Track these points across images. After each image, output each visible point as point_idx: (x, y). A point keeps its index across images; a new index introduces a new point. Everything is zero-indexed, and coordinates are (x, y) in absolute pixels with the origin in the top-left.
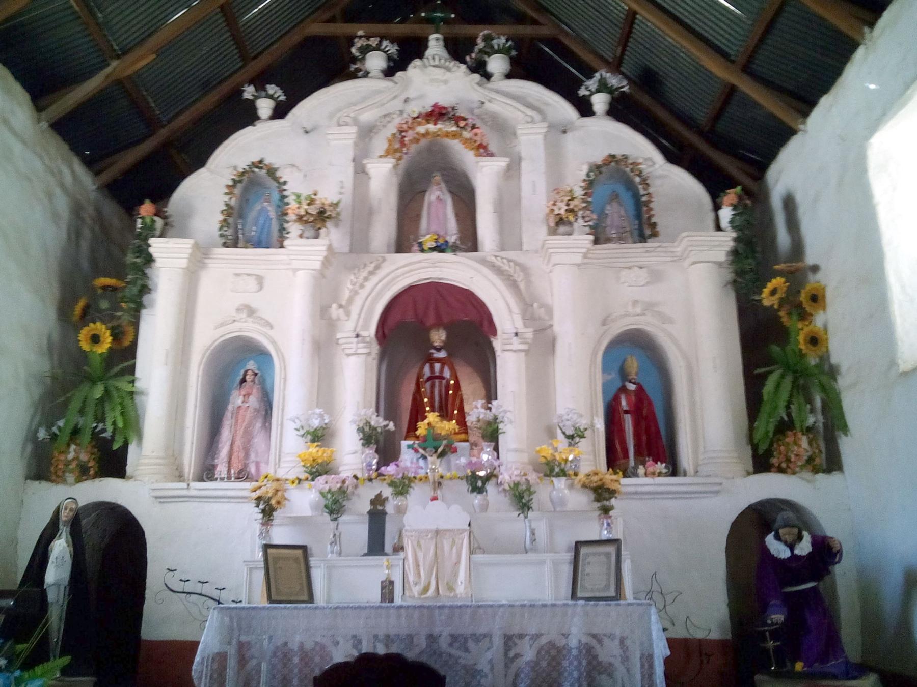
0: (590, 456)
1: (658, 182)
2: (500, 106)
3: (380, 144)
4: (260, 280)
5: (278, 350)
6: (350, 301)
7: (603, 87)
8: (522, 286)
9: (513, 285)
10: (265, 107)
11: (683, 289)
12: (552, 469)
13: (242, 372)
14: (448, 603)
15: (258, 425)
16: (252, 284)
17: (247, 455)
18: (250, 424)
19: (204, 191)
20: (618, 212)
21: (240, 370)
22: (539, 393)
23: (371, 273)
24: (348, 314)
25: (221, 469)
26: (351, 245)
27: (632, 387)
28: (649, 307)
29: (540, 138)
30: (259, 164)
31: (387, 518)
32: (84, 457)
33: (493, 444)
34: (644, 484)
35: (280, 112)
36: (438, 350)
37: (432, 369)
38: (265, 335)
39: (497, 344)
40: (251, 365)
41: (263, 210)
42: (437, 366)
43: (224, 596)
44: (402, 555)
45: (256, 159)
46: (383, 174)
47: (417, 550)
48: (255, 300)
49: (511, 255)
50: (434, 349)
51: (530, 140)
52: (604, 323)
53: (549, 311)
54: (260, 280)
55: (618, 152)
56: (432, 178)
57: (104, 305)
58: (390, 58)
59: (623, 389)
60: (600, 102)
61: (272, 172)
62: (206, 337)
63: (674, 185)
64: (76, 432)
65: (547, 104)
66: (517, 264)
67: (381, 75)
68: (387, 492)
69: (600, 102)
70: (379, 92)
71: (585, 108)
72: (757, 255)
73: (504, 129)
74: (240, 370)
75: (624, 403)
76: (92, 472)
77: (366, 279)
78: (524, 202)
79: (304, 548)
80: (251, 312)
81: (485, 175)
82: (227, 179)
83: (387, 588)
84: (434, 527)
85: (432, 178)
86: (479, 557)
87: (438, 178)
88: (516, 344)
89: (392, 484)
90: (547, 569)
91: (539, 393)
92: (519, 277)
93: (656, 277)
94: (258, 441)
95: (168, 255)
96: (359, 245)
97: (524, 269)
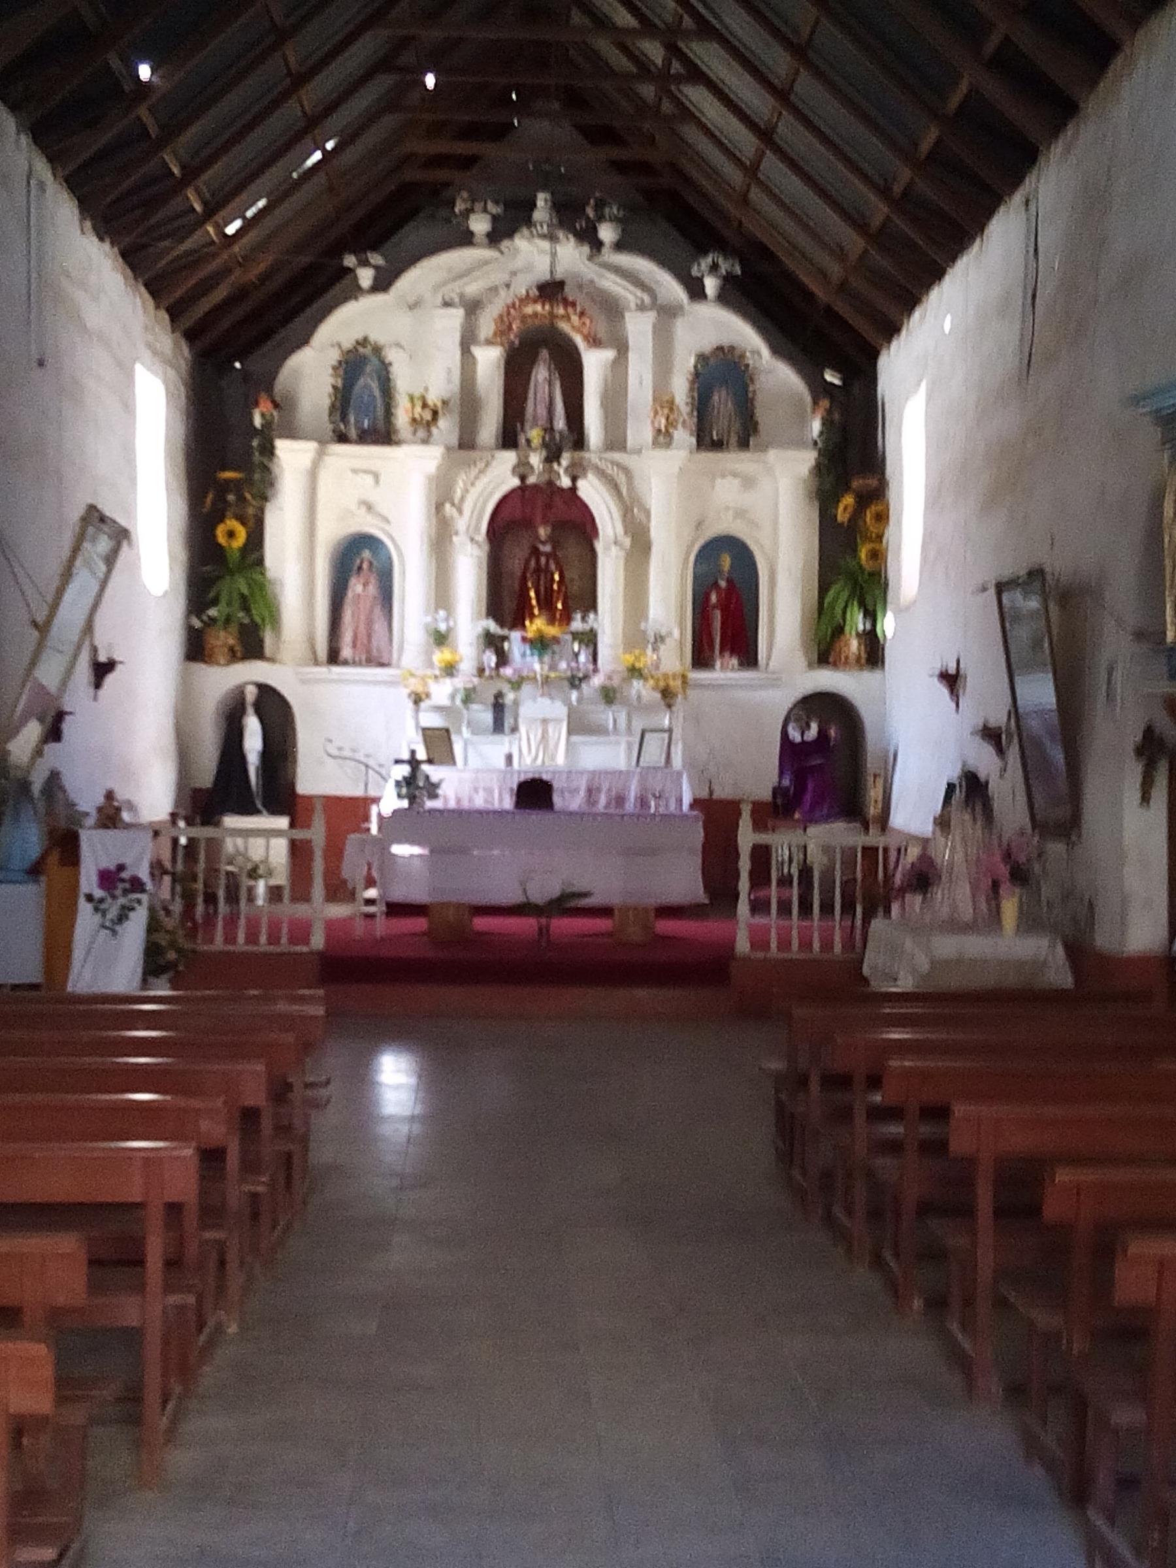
0: (673, 657)
1: (763, 378)
2: (611, 284)
3: (486, 325)
4: (376, 477)
5: (400, 555)
6: (462, 499)
7: (714, 268)
8: (624, 491)
9: (614, 487)
10: (366, 277)
11: (771, 500)
12: (634, 672)
13: (358, 561)
14: (551, 769)
15: (378, 611)
16: (369, 479)
17: (369, 641)
18: (371, 611)
19: (310, 371)
20: (722, 413)
21: (358, 561)
22: (642, 599)
23: (481, 472)
24: (460, 511)
25: (346, 652)
26: (461, 438)
27: (723, 584)
28: (740, 513)
29: (650, 328)
30: (364, 342)
31: (506, 710)
32: (231, 641)
33: (591, 650)
34: (724, 672)
35: (382, 284)
36: (543, 543)
37: (538, 561)
38: (383, 530)
39: (599, 546)
40: (366, 554)
41: (367, 386)
42: (543, 560)
43: (371, 763)
44: (517, 735)
45: (359, 336)
46: (489, 359)
47: (387, 527)
48: (374, 496)
49: (617, 456)
50: (538, 563)
51: (639, 327)
52: (699, 525)
53: (648, 513)
54: (376, 477)
55: (725, 341)
56: (540, 349)
57: (231, 497)
58: (495, 219)
59: (716, 585)
60: (711, 285)
61: (377, 350)
62: (330, 533)
63: (778, 377)
64: (228, 620)
65: (657, 282)
66: (618, 465)
67: (486, 241)
68: (506, 688)
69: (711, 285)
70: (486, 263)
71: (696, 291)
72: (255, 1094)
73: (613, 309)
74: (358, 561)
75: (714, 598)
76: (239, 654)
77: (477, 478)
78: (630, 396)
79: (447, 731)
80: (369, 507)
81: (595, 363)
82: (334, 356)
83: (509, 758)
84: (541, 716)
85: (540, 349)
86: (574, 738)
87: (544, 354)
88: (614, 550)
89: (509, 681)
90: (623, 746)
91: (642, 599)
92: (622, 479)
93: (748, 483)
94: (379, 627)
95: (292, 457)
96: (467, 442)
97: (626, 471)
